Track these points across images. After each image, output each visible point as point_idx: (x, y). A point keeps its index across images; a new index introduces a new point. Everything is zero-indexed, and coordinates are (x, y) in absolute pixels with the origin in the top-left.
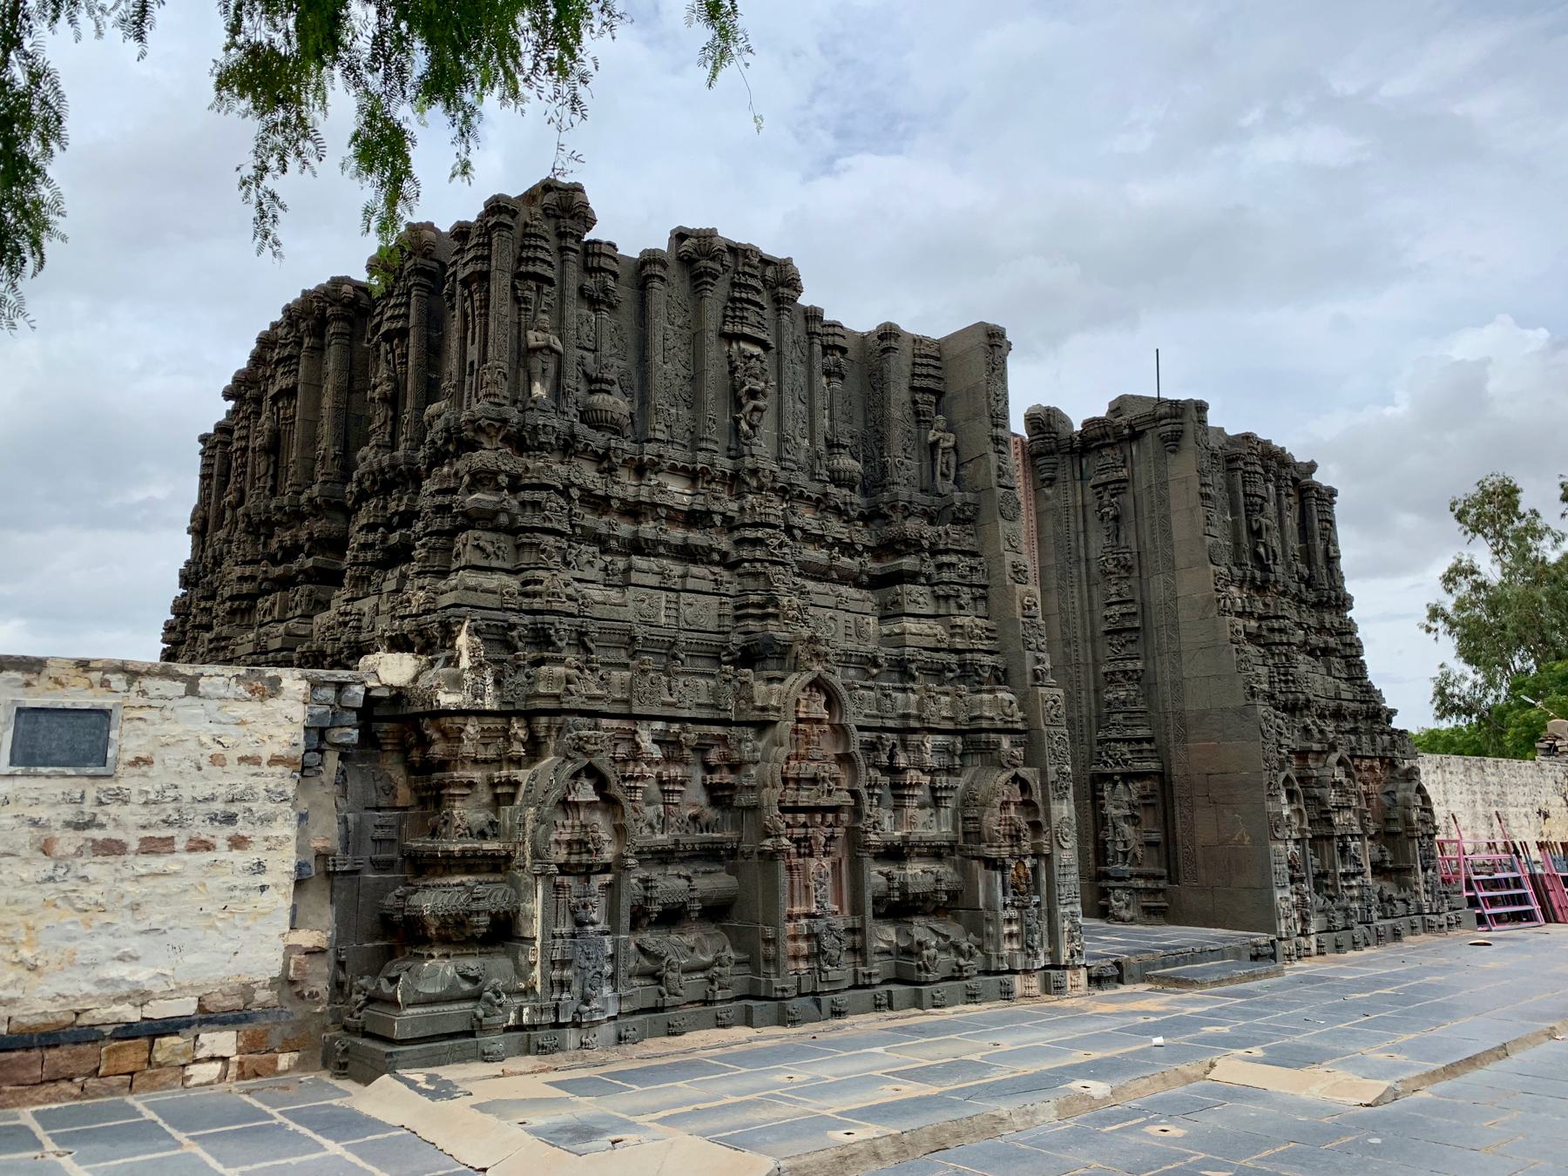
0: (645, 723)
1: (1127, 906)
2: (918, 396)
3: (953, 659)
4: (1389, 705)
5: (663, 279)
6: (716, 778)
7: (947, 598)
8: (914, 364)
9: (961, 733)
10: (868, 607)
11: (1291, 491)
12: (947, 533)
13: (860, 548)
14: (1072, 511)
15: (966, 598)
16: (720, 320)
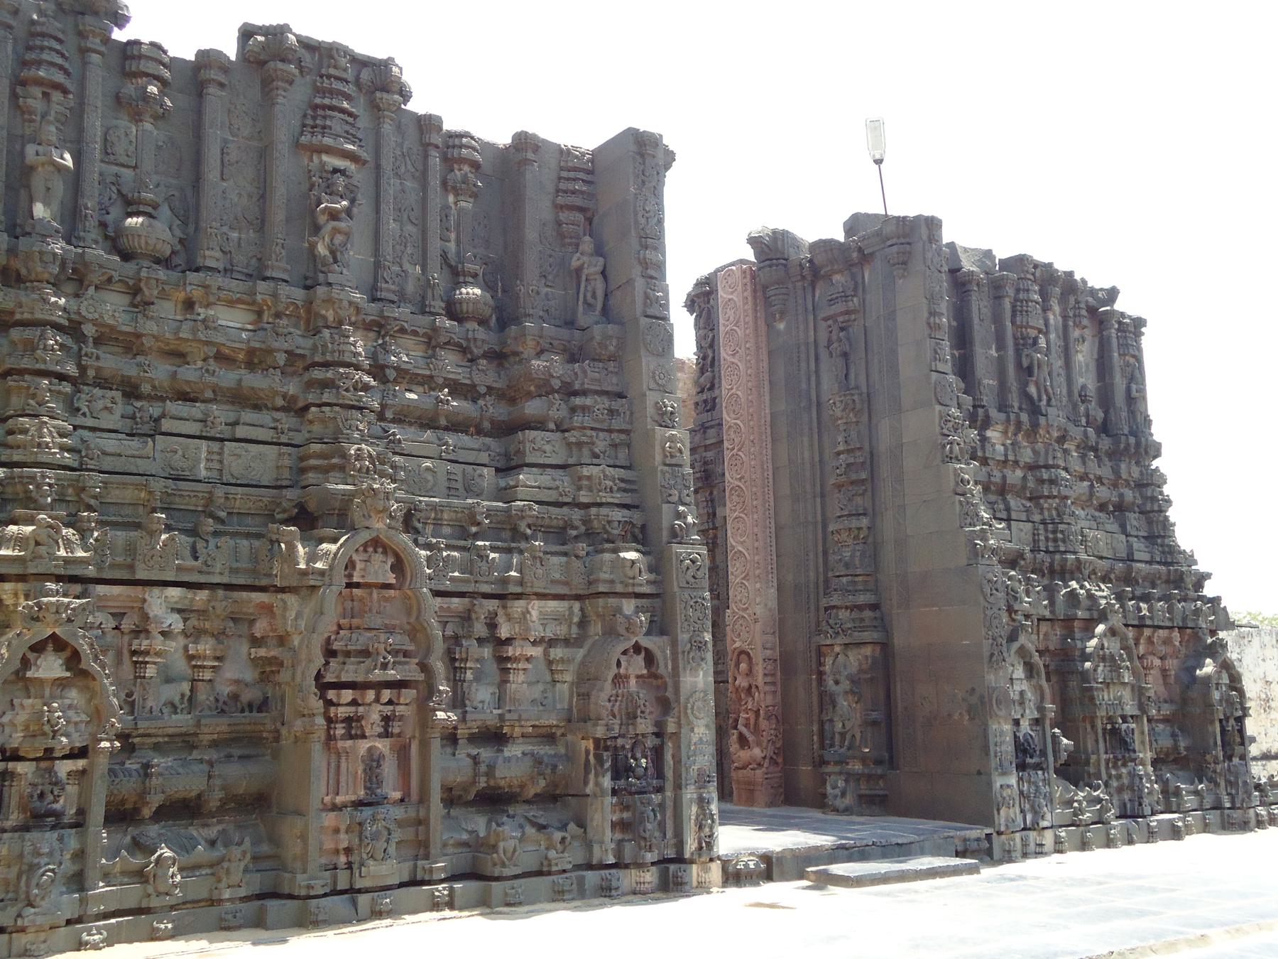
0: (156, 591)
1: (843, 794)
2: (563, 216)
3: (576, 515)
4: (1201, 567)
5: (222, 85)
6: (262, 652)
7: (580, 445)
8: (560, 178)
9: (578, 597)
10: (484, 457)
11: (1085, 322)
12: (585, 372)
13: (483, 390)
14: (803, 348)
15: (601, 444)
16: (298, 129)
